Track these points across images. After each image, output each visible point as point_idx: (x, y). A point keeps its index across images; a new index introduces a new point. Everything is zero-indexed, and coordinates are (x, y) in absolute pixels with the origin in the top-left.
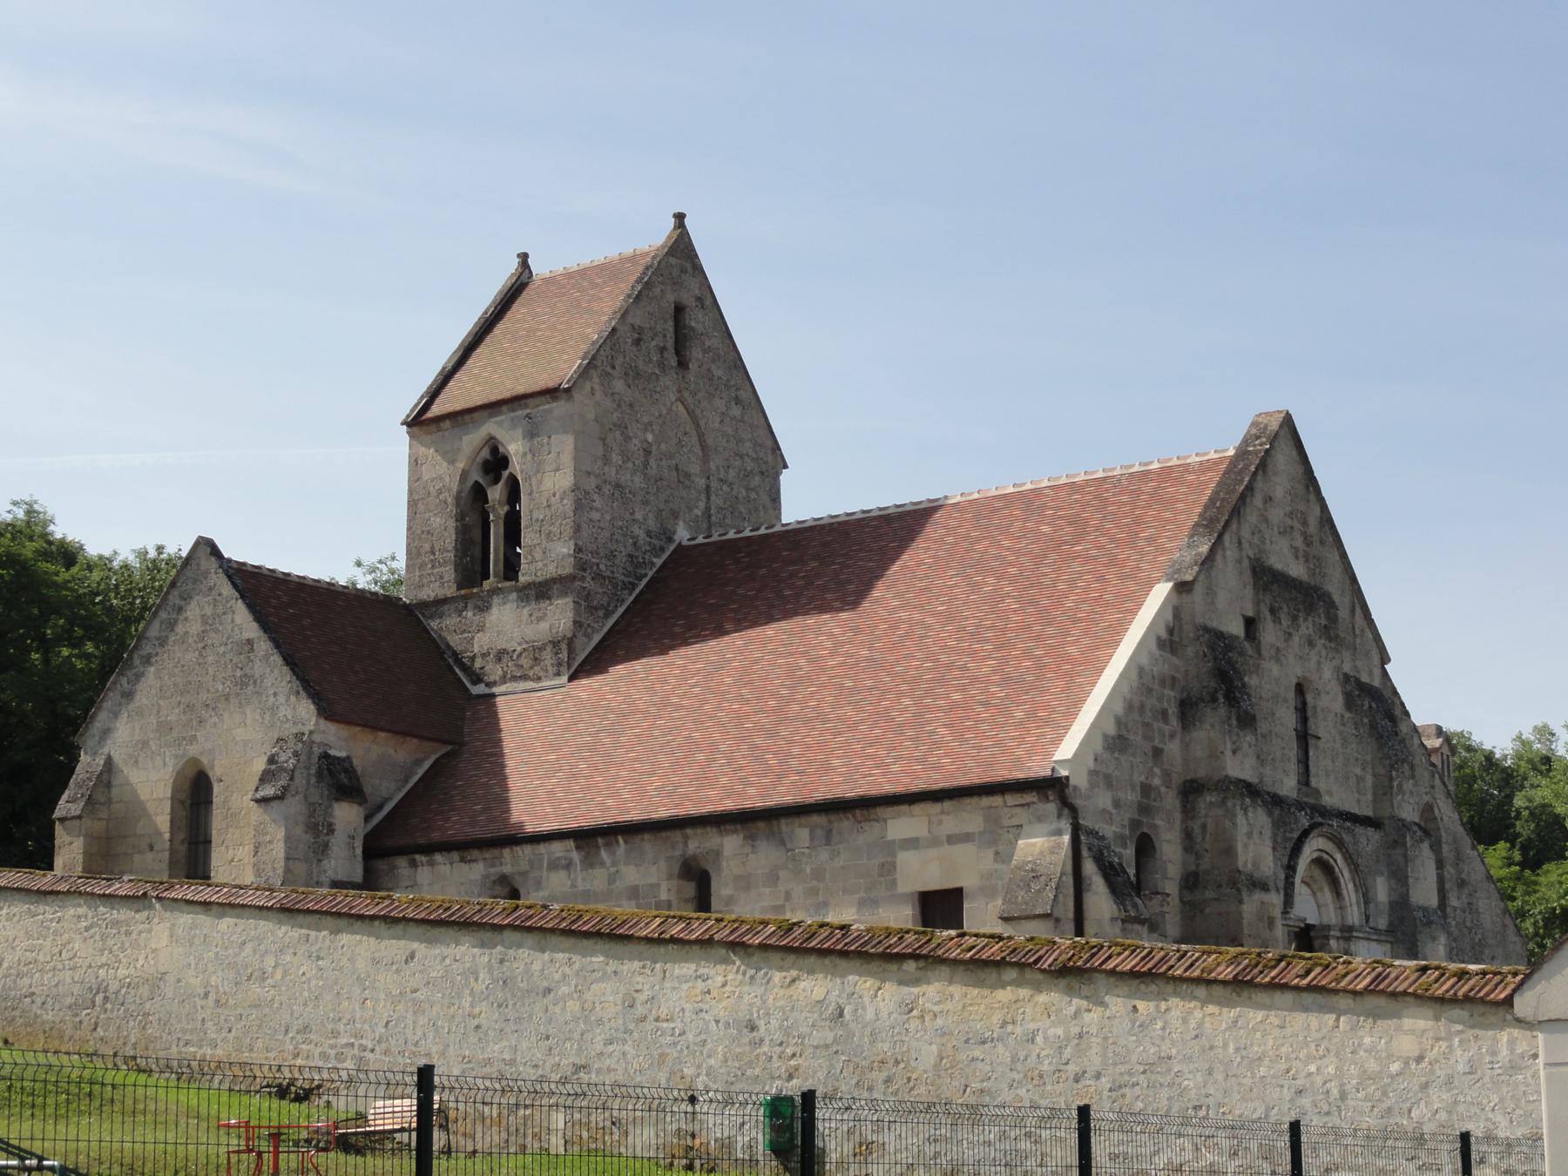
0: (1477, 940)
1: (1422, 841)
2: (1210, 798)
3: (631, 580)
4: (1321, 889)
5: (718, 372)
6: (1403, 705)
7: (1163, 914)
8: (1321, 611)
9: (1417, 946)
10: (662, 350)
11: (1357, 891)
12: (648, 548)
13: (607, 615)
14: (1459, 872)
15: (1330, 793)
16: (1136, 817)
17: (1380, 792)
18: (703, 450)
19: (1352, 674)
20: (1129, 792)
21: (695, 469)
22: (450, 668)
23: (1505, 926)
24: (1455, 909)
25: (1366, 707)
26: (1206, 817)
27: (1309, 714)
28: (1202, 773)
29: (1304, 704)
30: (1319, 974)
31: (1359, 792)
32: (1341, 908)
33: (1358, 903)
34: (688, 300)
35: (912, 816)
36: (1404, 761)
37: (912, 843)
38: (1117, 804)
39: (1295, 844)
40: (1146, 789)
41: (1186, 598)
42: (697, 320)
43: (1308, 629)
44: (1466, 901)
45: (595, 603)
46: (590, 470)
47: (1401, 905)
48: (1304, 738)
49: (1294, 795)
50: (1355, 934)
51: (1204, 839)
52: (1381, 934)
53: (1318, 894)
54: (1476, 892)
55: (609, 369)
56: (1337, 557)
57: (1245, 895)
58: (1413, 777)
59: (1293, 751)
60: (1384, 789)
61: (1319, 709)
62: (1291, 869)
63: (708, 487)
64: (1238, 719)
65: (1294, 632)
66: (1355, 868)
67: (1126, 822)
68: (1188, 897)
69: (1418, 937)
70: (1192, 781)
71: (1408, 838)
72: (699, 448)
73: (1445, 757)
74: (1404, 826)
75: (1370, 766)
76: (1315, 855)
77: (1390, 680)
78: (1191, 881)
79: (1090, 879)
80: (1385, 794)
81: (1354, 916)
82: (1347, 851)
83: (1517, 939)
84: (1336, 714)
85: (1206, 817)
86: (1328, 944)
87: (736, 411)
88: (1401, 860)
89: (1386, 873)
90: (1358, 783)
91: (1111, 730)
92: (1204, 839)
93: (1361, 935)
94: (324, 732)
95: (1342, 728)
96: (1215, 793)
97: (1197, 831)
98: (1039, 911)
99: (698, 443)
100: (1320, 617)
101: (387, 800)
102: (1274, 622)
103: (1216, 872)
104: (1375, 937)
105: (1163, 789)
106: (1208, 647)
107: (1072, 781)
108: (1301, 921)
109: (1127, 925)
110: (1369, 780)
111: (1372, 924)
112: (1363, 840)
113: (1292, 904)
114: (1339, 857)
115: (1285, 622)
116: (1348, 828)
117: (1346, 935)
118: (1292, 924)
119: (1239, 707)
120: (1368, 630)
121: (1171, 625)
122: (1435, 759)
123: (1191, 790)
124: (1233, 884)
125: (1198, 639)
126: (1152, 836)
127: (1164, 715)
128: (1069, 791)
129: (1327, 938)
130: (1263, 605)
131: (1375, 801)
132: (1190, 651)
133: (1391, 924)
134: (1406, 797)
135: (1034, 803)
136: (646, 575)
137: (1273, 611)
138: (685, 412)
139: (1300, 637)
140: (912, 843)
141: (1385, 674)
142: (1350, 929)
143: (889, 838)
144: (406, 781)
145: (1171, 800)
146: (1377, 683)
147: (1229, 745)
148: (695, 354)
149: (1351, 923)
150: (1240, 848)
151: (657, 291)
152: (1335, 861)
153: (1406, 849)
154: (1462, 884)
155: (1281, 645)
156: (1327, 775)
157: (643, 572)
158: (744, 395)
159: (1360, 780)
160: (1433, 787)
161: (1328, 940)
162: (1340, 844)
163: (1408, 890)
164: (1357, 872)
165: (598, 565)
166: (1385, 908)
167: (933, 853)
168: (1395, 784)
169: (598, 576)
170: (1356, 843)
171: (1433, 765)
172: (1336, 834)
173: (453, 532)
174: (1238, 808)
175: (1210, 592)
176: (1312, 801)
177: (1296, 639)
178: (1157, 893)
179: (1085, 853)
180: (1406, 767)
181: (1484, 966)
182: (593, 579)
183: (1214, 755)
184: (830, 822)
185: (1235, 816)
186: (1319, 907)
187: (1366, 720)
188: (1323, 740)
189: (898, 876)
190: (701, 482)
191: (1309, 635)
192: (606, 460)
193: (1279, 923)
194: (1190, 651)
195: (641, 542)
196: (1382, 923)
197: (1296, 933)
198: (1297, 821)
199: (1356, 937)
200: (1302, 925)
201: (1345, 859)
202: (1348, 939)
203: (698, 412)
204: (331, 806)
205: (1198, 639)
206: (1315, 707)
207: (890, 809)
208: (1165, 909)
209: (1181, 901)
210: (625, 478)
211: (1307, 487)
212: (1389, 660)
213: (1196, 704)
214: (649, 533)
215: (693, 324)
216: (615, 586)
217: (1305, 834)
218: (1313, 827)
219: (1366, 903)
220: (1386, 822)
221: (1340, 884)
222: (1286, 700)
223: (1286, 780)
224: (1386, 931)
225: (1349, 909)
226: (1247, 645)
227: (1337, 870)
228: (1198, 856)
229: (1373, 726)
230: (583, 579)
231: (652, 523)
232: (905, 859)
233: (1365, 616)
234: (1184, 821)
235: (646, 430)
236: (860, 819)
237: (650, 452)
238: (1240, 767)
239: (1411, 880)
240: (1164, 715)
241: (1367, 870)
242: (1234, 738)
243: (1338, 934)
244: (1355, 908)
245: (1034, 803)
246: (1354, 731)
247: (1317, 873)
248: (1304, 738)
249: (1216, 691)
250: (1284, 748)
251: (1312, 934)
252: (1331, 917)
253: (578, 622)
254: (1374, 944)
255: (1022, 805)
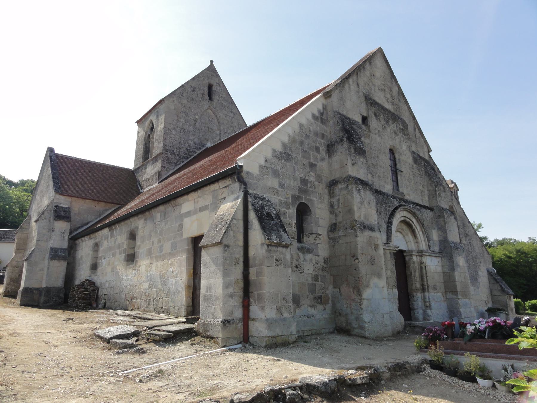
0: (474, 256)
1: (451, 215)
2: (340, 186)
3: (187, 156)
4: (407, 235)
5: (224, 104)
6: (438, 169)
7: (316, 244)
8: (400, 122)
9: (453, 258)
10: (203, 95)
11: (424, 235)
12: (194, 147)
13: (176, 165)
14: (465, 231)
15: (409, 195)
16: (297, 194)
17: (431, 197)
18: (219, 124)
19: (416, 152)
20: (292, 181)
21: (215, 128)
22: (137, 186)
23: (483, 251)
24: (465, 245)
25: (423, 164)
26: (339, 196)
27: (397, 162)
28: (337, 175)
29: (395, 158)
30: (180, 323)
31: (422, 196)
32: (417, 242)
33: (425, 241)
34: (212, 82)
35: (189, 201)
36: (440, 185)
37: (188, 214)
38: (282, 186)
39: (391, 212)
40: (304, 181)
41: (329, 100)
42: (215, 88)
43: (394, 127)
44: (468, 242)
45: (171, 161)
46: (171, 123)
47: (444, 242)
48: (395, 171)
49: (391, 193)
50: (424, 254)
51: (338, 206)
52: (436, 254)
53: (406, 237)
54: (472, 238)
55: (180, 96)
56: (406, 108)
57: (358, 232)
58: (445, 192)
59: (389, 174)
60: (433, 195)
61: (401, 161)
62: (389, 223)
63: (220, 134)
64: (355, 149)
65: (387, 127)
66: (422, 225)
67: (290, 196)
68: (331, 236)
69: (453, 254)
70: (333, 180)
71: (445, 214)
72: (218, 123)
73: (455, 191)
74: (442, 210)
75: (426, 186)
76: (402, 219)
77: (432, 159)
78: (333, 228)
79: (252, 222)
80: (433, 197)
81: (423, 246)
82: (418, 218)
83: (488, 256)
84: (410, 164)
85: (339, 196)
86: (412, 258)
87: (232, 115)
88: (443, 223)
89: (436, 229)
90: (421, 192)
91: (279, 148)
92: (338, 206)
93: (427, 254)
94: (58, 199)
95: (413, 170)
96: (343, 183)
97: (336, 203)
98: (216, 241)
99: (217, 122)
100: (399, 125)
101: (90, 222)
102: (377, 119)
103: (345, 222)
104: (434, 255)
105: (316, 183)
106: (339, 119)
107: (245, 169)
108: (396, 247)
109: (270, 248)
110: (426, 192)
111: (432, 249)
112: (425, 214)
113: (391, 239)
114: (414, 220)
115: (383, 122)
116: (418, 209)
117: (420, 254)
118: (392, 249)
119: (355, 145)
120: (421, 138)
121: (322, 111)
122: (453, 190)
123: (332, 184)
124: (352, 227)
125: (334, 117)
126: (309, 205)
127: (317, 149)
128: (244, 174)
129: (411, 255)
130: (370, 111)
131: (429, 200)
132: (331, 123)
133: (440, 249)
134: (443, 199)
135: (231, 184)
136: (193, 155)
137: (376, 115)
138: (212, 112)
139: (391, 130)
140: (188, 214)
141: (430, 156)
142: (422, 251)
143: (182, 213)
144: (100, 215)
145: (322, 189)
146: (427, 158)
147: (350, 161)
148: (215, 97)
149: (422, 249)
150: (356, 208)
151: (202, 79)
152: (413, 222)
153: (445, 219)
154: (466, 235)
155: (381, 130)
156: (407, 187)
157: (192, 154)
158: (234, 111)
159: (422, 192)
160: (452, 199)
161: (412, 256)
162: (414, 215)
163: (447, 235)
164: (423, 227)
165: (173, 150)
166: (438, 243)
167: (194, 217)
168: (438, 193)
169: (173, 154)
170: (422, 215)
171: (452, 192)
172: (412, 210)
173: (143, 148)
174: (354, 189)
175: (342, 99)
176: (400, 197)
177: (388, 130)
178: (312, 234)
179: (250, 207)
180: (441, 187)
181: (35, 241)
182: (171, 154)
183: (343, 166)
184: (165, 209)
185: (353, 193)
186: (407, 242)
187: (423, 169)
188: (404, 173)
189: (183, 231)
190: (218, 132)
191: (395, 130)
192: (178, 121)
193: (381, 247)
194: (331, 123)
195: (192, 146)
196: (437, 249)
197: (394, 253)
198: (392, 203)
199: (425, 255)
200: (397, 249)
201: (418, 221)
202: (421, 256)
203: (216, 113)
204: (54, 223)
205: (334, 117)
206: (399, 159)
207: (181, 199)
208: (317, 242)
209: (329, 238)
210: (186, 127)
211: (392, 79)
212: (431, 151)
213: (334, 145)
214: (195, 143)
215: (215, 89)
216: (180, 157)
217: (396, 208)
218: (400, 206)
219: (429, 240)
220: (435, 208)
221: (416, 233)
222: (384, 153)
223: (386, 186)
224: (438, 252)
225: (421, 243)
226: (363, 126)
227: (414, 226)
228: (336, 216)
229: (426, 172)
230: (166, 154)
231: (196, 140)
232: (187, 221)
233: (420, 133)
234: (330, 199)
235: (195, 115)
236: (173, 205)
237: (197, 121)
238: (353, 172)
239: (448, 231)
240: (317, 149)
241: (428, 227)
242: (353, 158)
243: (416, 254)
244: (423, 243)
245: (231, 184)
246: (418, 173)
247: (405, 227)
248: (395, 171)
249: (343, 137)
250: (384, 172)
251: (405, 254)
252: (412, 246)
253: (163, 166)
254: (433, 258)
255: (226, 187)
